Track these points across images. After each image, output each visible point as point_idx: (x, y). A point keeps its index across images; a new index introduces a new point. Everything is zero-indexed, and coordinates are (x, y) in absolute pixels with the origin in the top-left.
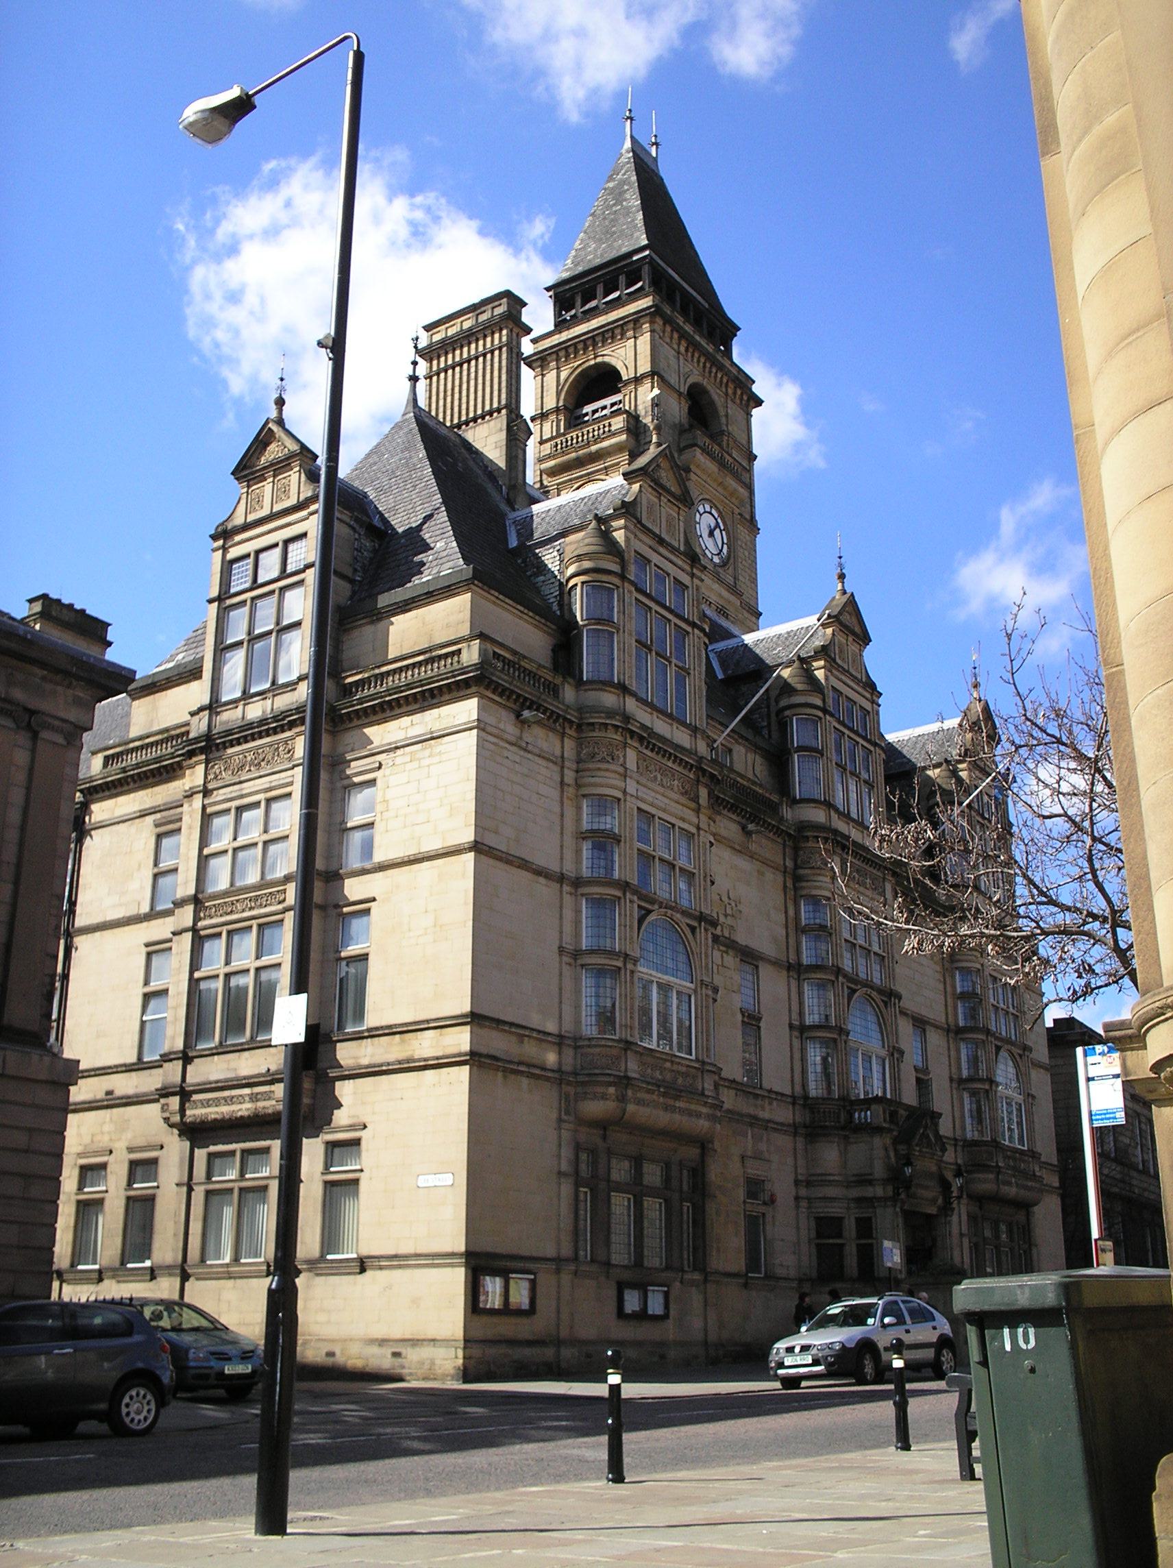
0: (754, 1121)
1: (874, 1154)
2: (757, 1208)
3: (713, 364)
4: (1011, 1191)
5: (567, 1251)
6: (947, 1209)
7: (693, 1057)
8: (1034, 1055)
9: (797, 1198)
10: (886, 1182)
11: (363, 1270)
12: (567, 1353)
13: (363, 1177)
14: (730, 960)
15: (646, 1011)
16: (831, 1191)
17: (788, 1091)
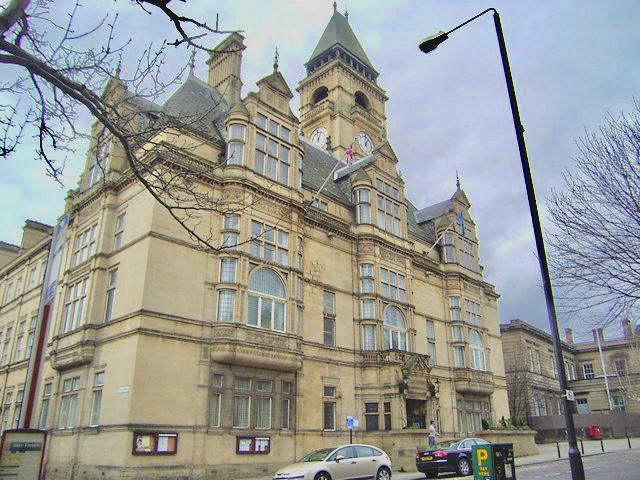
0: (329, 362)
1: (391, 375)
2: (329, 399)
4: (477, 388)
5: (202, 421)
10: (395, 386)
11: (99, 432)
14: (318, 290)
16: (373, 392)
17: (352, 348)
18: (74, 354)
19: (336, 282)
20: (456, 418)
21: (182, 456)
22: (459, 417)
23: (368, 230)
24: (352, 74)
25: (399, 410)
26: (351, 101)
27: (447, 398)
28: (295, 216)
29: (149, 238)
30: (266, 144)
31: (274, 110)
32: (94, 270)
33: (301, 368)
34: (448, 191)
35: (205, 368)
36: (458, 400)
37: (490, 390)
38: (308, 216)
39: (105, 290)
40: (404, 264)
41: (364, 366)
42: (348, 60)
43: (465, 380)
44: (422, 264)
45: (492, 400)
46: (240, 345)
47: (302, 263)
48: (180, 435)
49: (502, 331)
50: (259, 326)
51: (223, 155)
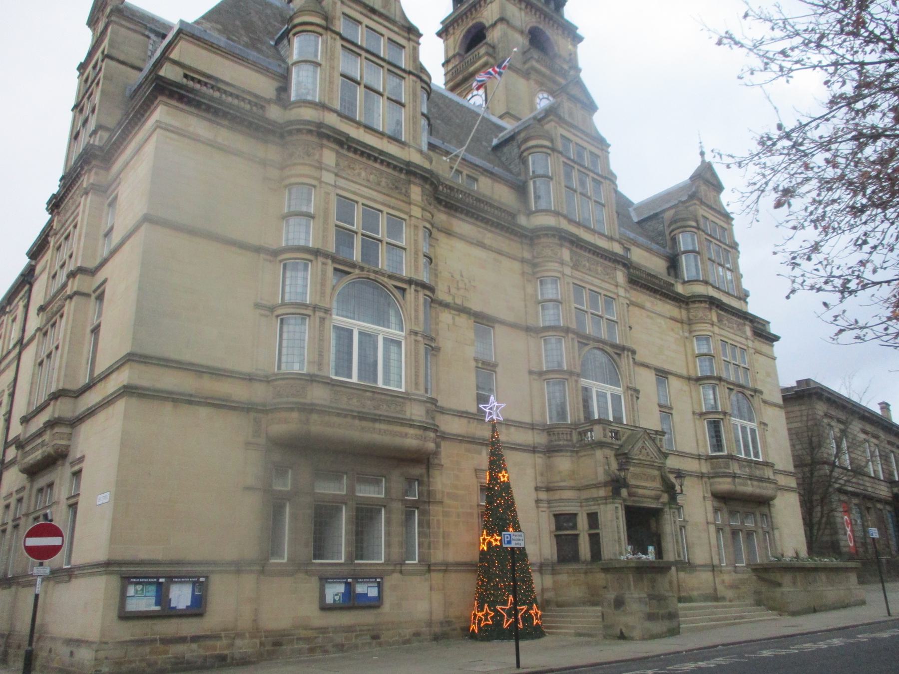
1: (598, 465)
4: (749, 488)
9: (538, 501)
14: (463, 321)
15: (738, 441)
18: (43, 444)
19: (495, 308)
20: (714, 541)
21: (212, 621)
22: (718, 539)
25: (613, 521)
27: (696, 504)
30: (356, 67)
31: (373, 11)
32: (70, 297)
33: (436, 454)
34: (677, 173)
36: (716, 510)
38: (446, 199)
39: (89, 328)
40: (614, 278)
41: (550, 450)
43: (726, 475)
44: (641, 281)
45: (773, 509)
47: (435, 273)
49: (786, 399)
51: (284, 88)
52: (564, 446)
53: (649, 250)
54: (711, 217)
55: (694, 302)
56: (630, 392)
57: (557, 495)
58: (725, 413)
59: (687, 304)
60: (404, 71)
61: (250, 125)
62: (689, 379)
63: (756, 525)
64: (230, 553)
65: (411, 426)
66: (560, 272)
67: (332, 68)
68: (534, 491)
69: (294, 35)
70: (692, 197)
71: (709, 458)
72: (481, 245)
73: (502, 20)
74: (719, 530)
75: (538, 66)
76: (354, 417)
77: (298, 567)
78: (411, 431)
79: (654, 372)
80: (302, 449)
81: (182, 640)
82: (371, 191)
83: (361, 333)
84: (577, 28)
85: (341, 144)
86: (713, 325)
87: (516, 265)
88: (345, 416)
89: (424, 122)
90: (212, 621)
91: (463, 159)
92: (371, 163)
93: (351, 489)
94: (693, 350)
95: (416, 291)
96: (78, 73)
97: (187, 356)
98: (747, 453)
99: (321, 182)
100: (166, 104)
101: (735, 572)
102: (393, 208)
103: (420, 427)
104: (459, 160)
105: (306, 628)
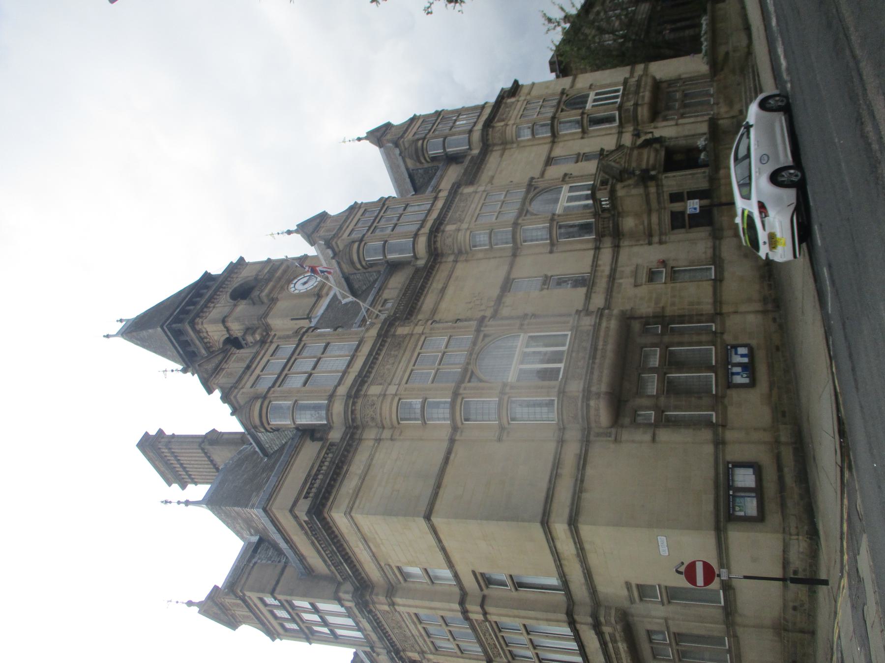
0: (612, 277)
1: (630, 196)
3: (221, 287)
6: (659, 140)
7: (569, 333)
8: (567, 87)
9: (661, 242)
10: (646, 187)
12: (785, 436)
13: (663, 584)
14: (508, 300)
17: (592, 252)
18: (614, 641)
20: (692, 120)
21: (754, 343)
23: (422, 241)
24: (206, 306)
26: (242, 307)
28: (402, 330)
29: (434, 519)
31: (248, 367)
32: (485, 614)
35: (625, 435)
36: (665, 119)
37: (650, 81)
39: (514, 594)
40: (470, 194)
41: (617, 235)
42: (184, 312)
46: (589, 386)
48: (729, 458)
50: (561, 366)
52: (613, 223)
53: (442, 177)
54: (414, 130)
55: (487, 140)
56: (567, 179)
57: (655, 227)
58: (583, 113)
59: (488, 146)
60: (298, 345)
61: (334, 479)
62: (514, 255)
63: (677, 91)
64: (708, 449)
65: (600, 324)
66: (392, 400)
67: (298, 391)
68: (651, 247)
69: (269, 424)
70: (397, 145)
71: (621, 125)
72: (443, 290)
73: (224, 321)
74: (682, 116)
75: (266, 291)
76: (594, 363)
77: (718, 402)
78: (604, 324)
79: (548, 168)
80: (621, 404)
81: (781, 479)
82: (403, 361)
83: (522, 363)
84: (232, 263)
85: (363, 382)
86: (507, 125)
87: (459, 266)
88: (593, 368)
89: (340, 330)
90: (766, 459)
91: (371, 306)
92: (378, 362)
93: (653, 370)
94: (528, 140)
95: (486, 326)
96: (278, 640)
97: (544, 485)
98: (617, 97)
99: (396, 395)
100: (330, 509)
101: (717, 104)
102: (416, 345)
103: (601, 319)
104: (371, 309)
105: (770, 396)
